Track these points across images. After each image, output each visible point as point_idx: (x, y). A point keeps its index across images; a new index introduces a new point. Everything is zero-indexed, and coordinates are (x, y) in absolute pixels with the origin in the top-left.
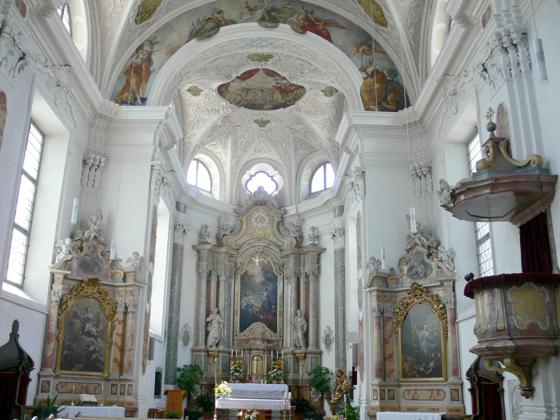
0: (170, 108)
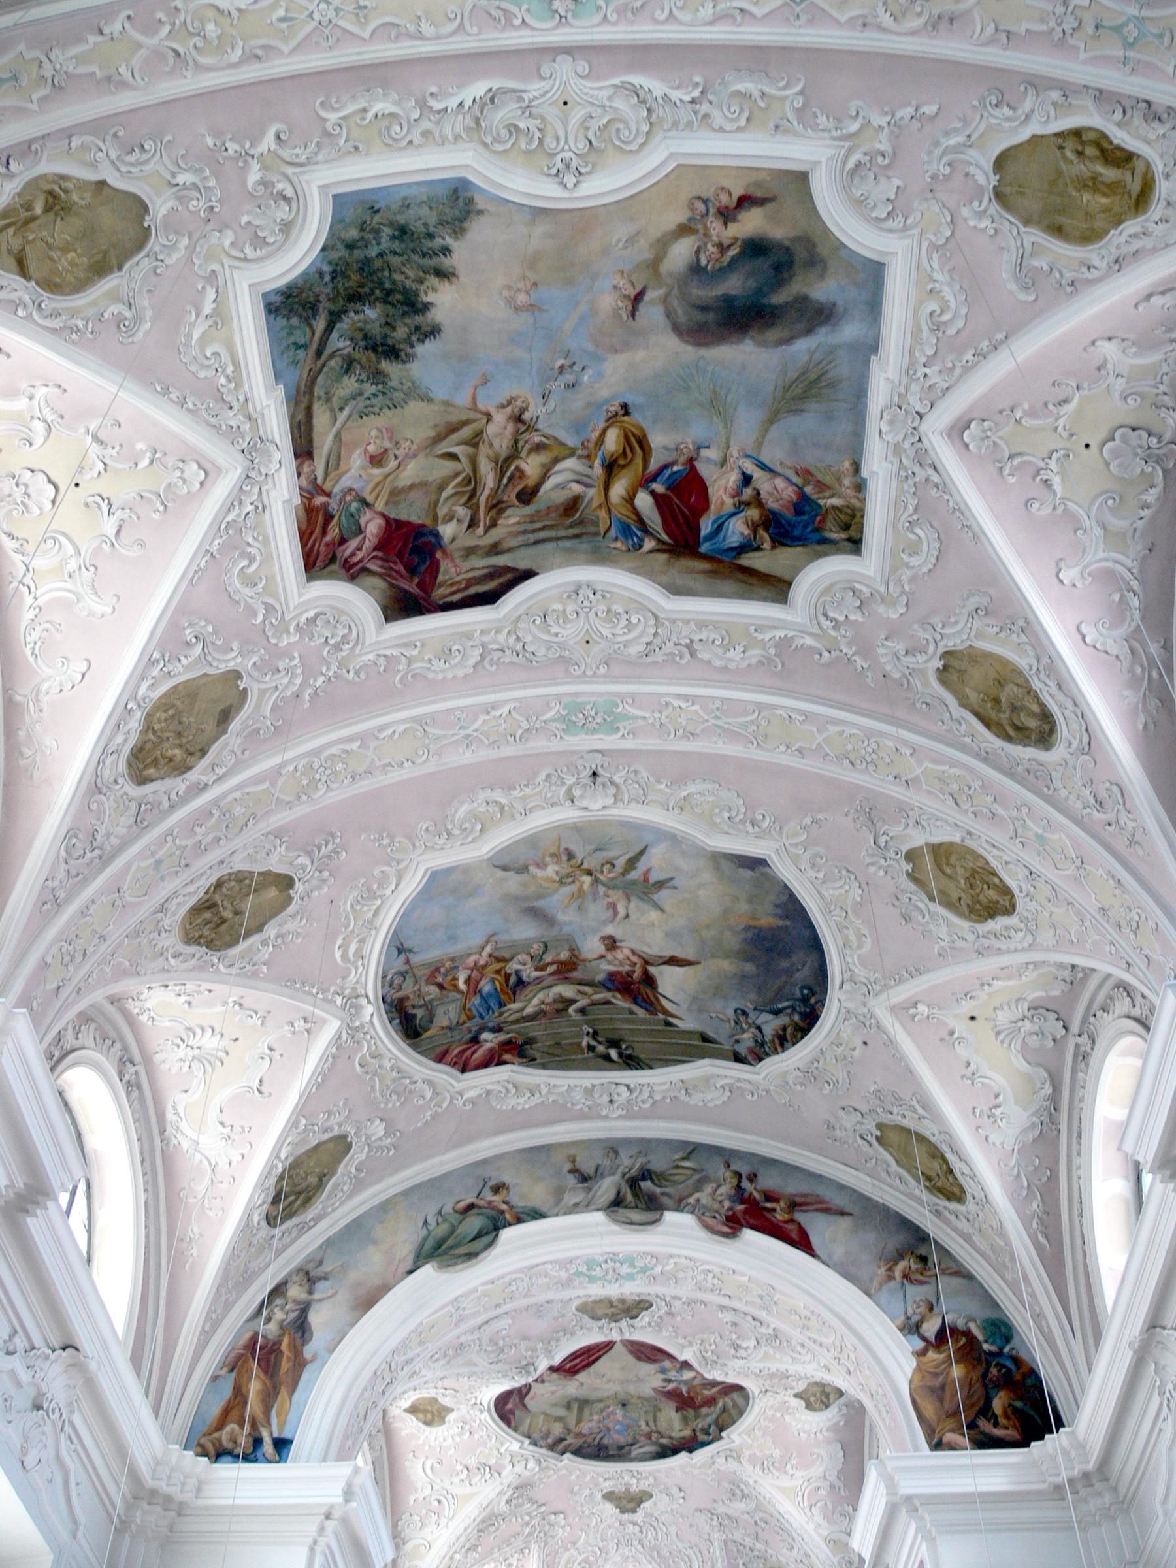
0: (357, 1470)
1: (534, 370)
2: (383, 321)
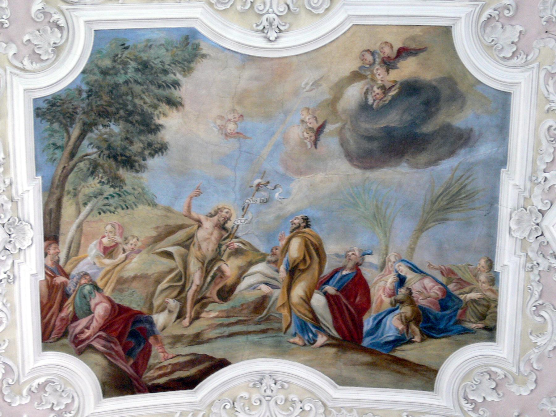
1: (237, 188)
2: (124, 135)
